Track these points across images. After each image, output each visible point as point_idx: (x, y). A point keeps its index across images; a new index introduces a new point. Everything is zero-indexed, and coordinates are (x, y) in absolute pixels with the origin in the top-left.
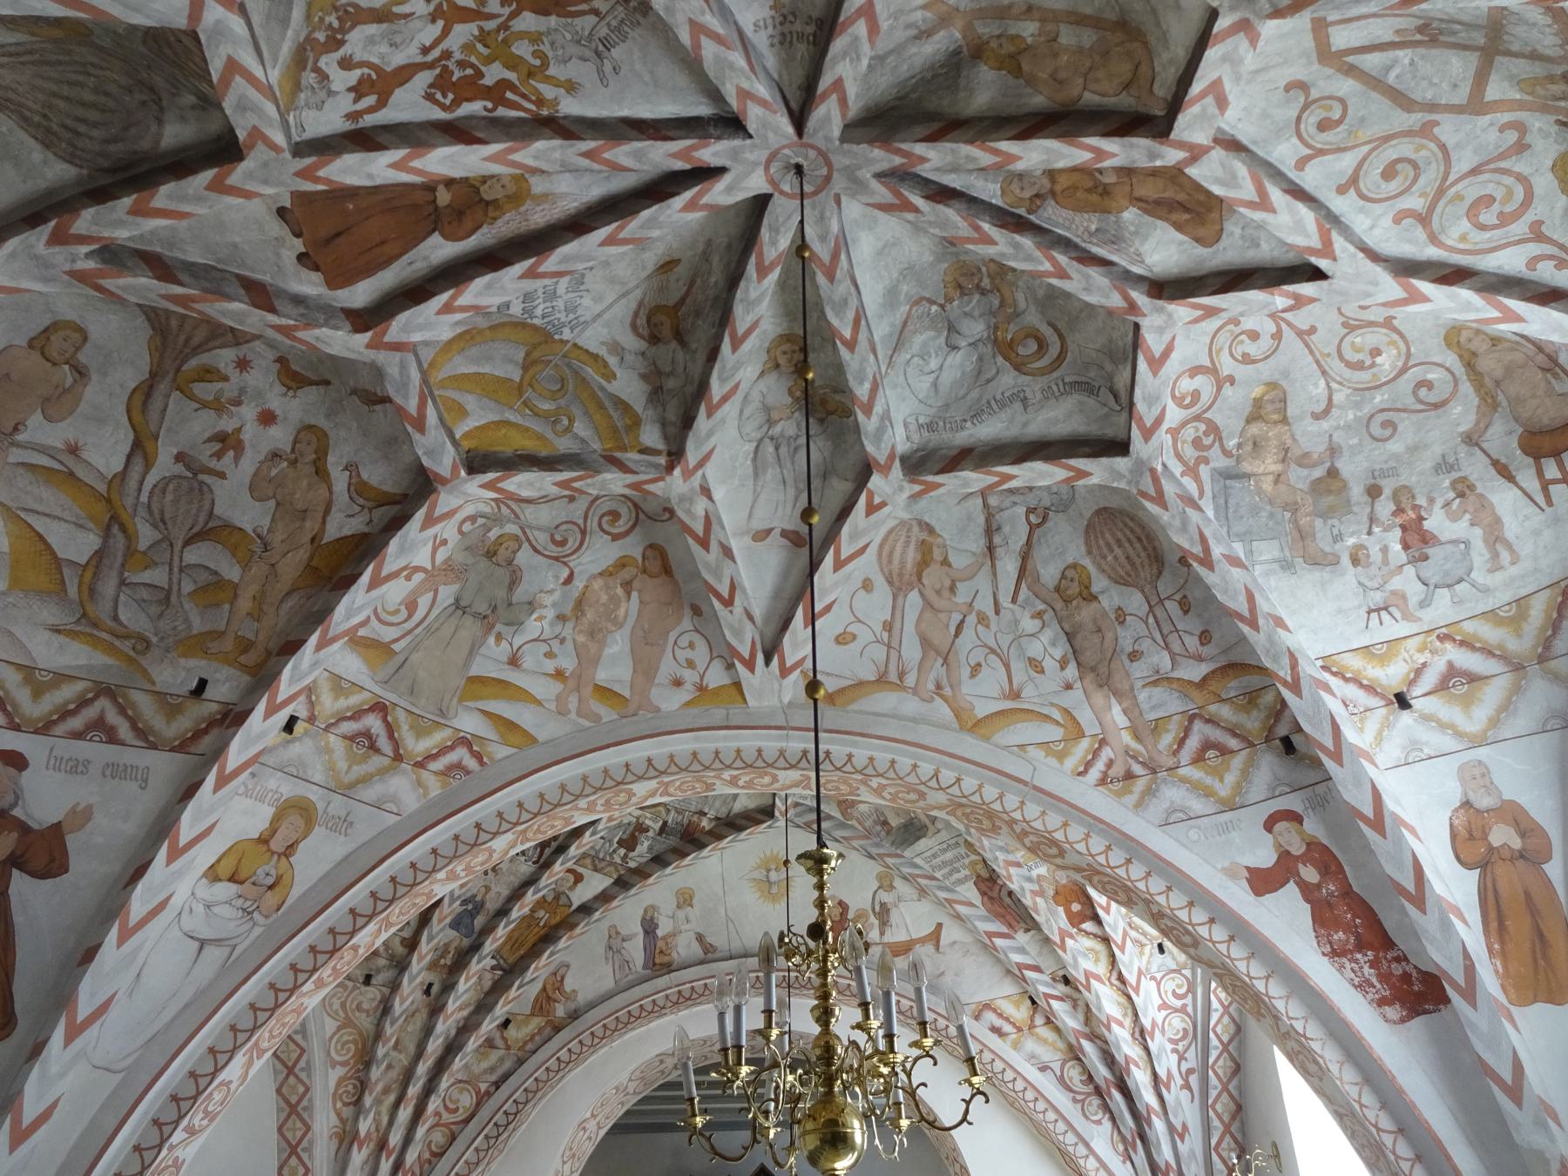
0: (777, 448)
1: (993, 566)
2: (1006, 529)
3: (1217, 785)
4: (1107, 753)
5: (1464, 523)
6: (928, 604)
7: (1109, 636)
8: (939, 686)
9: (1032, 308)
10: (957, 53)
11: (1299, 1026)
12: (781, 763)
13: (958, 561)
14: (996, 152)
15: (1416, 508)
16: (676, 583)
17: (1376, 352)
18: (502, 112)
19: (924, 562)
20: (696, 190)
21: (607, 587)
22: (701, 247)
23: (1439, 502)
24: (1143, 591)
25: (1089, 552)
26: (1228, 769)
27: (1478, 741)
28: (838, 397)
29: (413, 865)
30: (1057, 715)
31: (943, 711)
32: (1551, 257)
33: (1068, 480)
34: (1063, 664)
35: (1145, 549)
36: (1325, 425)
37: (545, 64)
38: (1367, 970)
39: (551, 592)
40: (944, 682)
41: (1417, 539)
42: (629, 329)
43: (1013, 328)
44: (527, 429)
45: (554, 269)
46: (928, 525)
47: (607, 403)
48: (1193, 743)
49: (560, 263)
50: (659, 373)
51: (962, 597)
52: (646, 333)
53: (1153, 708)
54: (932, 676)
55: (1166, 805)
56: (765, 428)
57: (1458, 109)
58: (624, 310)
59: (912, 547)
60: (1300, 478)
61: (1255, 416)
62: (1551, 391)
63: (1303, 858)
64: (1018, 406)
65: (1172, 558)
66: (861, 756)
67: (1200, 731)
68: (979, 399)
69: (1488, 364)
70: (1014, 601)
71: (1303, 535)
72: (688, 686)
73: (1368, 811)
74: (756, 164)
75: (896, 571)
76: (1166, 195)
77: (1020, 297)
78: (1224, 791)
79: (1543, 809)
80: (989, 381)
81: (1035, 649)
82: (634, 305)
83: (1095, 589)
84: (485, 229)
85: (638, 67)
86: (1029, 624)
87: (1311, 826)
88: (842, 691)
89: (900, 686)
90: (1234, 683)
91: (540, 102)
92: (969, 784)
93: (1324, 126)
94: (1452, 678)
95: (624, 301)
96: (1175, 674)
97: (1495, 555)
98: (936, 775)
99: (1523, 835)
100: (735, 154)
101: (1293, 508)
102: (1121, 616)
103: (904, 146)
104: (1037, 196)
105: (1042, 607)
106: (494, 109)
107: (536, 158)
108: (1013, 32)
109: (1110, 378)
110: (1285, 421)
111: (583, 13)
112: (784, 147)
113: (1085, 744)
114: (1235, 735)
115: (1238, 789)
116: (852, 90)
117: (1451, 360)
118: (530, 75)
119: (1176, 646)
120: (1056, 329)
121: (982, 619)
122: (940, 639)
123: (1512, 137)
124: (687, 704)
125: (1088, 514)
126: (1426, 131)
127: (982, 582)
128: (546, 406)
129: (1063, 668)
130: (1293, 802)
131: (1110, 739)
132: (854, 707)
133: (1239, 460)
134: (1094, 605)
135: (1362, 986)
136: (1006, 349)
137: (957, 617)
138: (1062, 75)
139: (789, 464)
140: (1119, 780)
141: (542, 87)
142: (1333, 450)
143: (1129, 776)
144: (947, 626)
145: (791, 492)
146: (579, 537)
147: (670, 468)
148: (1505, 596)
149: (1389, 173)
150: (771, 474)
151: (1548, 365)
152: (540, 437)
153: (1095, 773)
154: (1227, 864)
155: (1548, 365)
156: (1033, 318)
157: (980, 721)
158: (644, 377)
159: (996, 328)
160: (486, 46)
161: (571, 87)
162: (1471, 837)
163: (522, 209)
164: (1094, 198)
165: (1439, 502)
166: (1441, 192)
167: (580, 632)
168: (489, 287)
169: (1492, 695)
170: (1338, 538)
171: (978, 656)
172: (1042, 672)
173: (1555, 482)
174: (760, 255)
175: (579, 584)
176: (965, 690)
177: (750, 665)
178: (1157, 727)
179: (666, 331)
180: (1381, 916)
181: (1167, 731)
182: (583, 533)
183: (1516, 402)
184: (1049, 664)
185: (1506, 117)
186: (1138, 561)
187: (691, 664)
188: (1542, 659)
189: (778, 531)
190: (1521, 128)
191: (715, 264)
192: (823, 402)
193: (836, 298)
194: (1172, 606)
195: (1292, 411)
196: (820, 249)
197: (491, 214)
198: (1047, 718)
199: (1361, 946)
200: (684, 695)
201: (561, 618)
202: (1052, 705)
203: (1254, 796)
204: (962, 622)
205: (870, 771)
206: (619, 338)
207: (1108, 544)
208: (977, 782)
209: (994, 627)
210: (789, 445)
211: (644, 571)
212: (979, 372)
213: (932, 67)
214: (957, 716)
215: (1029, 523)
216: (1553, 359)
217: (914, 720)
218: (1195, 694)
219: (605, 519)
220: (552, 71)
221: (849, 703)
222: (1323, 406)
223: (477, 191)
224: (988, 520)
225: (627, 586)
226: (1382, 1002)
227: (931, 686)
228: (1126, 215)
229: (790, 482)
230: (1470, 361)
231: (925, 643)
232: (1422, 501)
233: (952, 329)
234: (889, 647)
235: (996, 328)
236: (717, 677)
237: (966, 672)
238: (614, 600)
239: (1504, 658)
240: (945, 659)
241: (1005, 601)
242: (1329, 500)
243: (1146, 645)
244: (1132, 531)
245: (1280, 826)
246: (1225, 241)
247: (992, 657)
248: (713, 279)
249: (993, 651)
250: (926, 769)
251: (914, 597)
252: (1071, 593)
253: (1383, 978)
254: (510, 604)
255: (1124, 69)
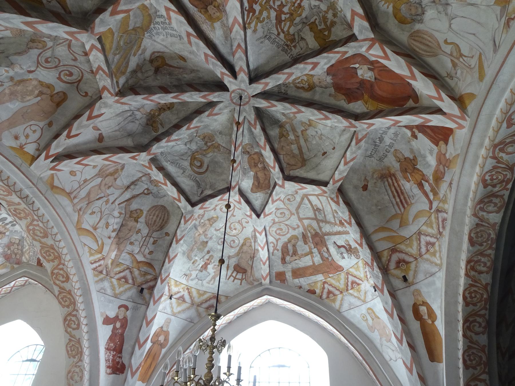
0: (130, 116)
1: (124, 192)
2: (137, 187)
3: (117, 289)
4: (102, 262)
5: (213, 271)
6: (100, 185)
7: (131, 233)
8: (80, 209)
9: (209, 159)
10: (279, 121)
11: (86, 365)
12: (18, 194)
13: (119, 182)
14: (265, 145)
15: (211, 261)
16: (55, 111)
17: (235, 229)
18: (246, 13)
19: (111, 174)
20: (229, 74)
21: (35, 87)
22: (195, 69)
23: (214, 264)
24: (149, 231)
25: (148, 211)
26: (123, 287)
27: (174, 314)
28: (159, 126)
29: (9, 177)
30: (100, 243)
31: (75, 218)
32: (274, 245)
33: (175, 198)
34: (114, 231)
35: (162, 223)
36: (215, 232)
37: (261, 22)
38: (111, 357)
39: (22, 68)
40: (83, 209)
41: (205, 267)
42: (153, 51)
43: (200, 156)
44: (112, 43)
45: (192, 41)
46: (124, 167)
47: (127, 59)
48: (122, 275)
49: (195, 42)
50: (141, 69)
51: (109, 192)
52: (153, 57)
53: (123, 259)
54: (82, 205)
55: (102, 286)
56: (136, 109)
57: (299, 217)
58: (159, 47)
59: (115, 168)
60: (203, 238)
61: (209, 220)
62: (247, 262)
63: (120, 320)
64: (182, 171)
65: (165, 230)
66: (42, 211)
67: (127, 272)
68: (176, 160)
69: (245, 248)
70: (119, 204)
71: (192, 250)
72: (18, 142)
73: (149, 319)
74: (240, 86)
75: (104, 169)
76: (261, 179)
77: (210, 154)
78: (117, 291)
79: (172, 337)
80: (182, 159)
81: (111, 221)
82: (162, 50)
83: (139, 220)
84: (195, 9)
85: (264, 49)
86: (116, 214)
87: (129, 313)
88: (57, 188)
89: (72, 200)
90: (145, 268)
91: (250, 23)
92: (62, 244)
93: (289, 200)
94: (182, 299)
95: (163, 47)
96: (136, 256)
97: (211, 280)
98: (56, 235)
99: (165, 340)
100: (243, 81)
101: (196, 242)
102: (139, 231)
103: (258, 123)
104: (248, 152)
105: (123, 212)
106: (246, 10)
107: (237, 32)
108: (289, 133)
109: (206, 189)
110: (211, 225)
111: (278, 30)
112: (247, 92)
113: (99, 256)
114: (133, 280)
115: (121, 293)
116: (273, 109)
117: (242, 242)
118: (258, 18)
119: (142, 250)
120: (208, 168)
121: (107, 202)
122: (93, 197)
123: (296, 227)
124: (12, 148)
125: (159, 204)
126: (292, 214)
127: (117, 193)
128: (122, 43)
129: (112, 232)
130: (130, 305)
131: (106, 259)
132: (57, 196)
133: (199, 225)
134: (135, 223)
135: (107, 361)
136: (193, 158)
137: (102, 195)
138: (284, 148)
139: (126, 122)
140: (98, 271)
141: (254, 23)
142: (211, 238)
143: (101, 272)
144: (98, 195)
145: (117, 128)
146: (54, 66)
147: (117, 95)
148: (204, 289)
149: (281, 213)
150: (120, 119)
151: (252, 257)
152: (111, 49)
153: (94, 266)
154: (103, 311)
155: (252, 257)
156: (206, 161)
157: (81, 228)
158: (138, 65)
159: (197, 152)
160: (265, 3)
161: (255, 31)
162: (157, 336)
163: (207, 21)
164: (253, 164)
165: (214, 264)
166: (280, 222)
167: (10, 89)
168: (181, 22)
169: (184, 306)
170: (196, 256)
171: (96, 210)
172: (107, 228)
173: (233, 276)
174: (209, 95)
175: (31, 76)
176: (85, 216)
177: (47, 157)
178: (119, 264)
179: (156, 64)
180: (124, 344)
181: (120, 267)
182: (56, 67)
183: (241, 258)
184: (111, 228)
185: (300, 224)
186: (157, 223)
187: (27, 136)
188: (198, 306)
189: (100, 132)
190: (298, 227)
191: (192, 75)
192: (154, 122)
193: (203, 119)
194: (152, 240)
195: (214, 225)
196: (216, 109)
197: (202, 10)
198: (97, 241)
199: (114, 350)
200: (14, 144)
201: (12, 79)
202: (102, 239)
203: (122, 298)
204: (102, 197)
205: (41, 218)
206: (148, 50)
207: (155, 214)
208: (64, 245)
209: (107, 206)
210: (133, 119)
211: (52, 96)
212: (183, 155)
213: (273, 116)
214: (77, 222)
215: (144, 191)
216: (254, 257)
217: (67, 214)
218: (135, 264)
219: (67, 72)
220: (259, 24)
221: (58, 193)
222: (218, 229)
223: (211, 4)
224: (137, 180)
225: (41, 93)
226: (108, 367)
227: (78, 208)
228: (252, 173)
229: (120, 126)
230: (244, 244)
231: (89, 194)
232: (212, 261)
233: (191, 141)
234: (80, 186)
235: (197, 152)
236: (31, 149)
237: (90, 211)
238: (32, 91)
239: (192, 301)
240: (88, 204)
241: (117, 202)
242: (201, 247)
243: (137, 243)
244: (164, 217)
245: (123, 309)
246: (254, 194)
247: (100, 213)
248: (185, 76)
249: (101, 212)
250: (55, 230)
251: (100, 180)
252: (134, 216)
253: (113, 360)
254: (7, 57)
255: (292, 162)
